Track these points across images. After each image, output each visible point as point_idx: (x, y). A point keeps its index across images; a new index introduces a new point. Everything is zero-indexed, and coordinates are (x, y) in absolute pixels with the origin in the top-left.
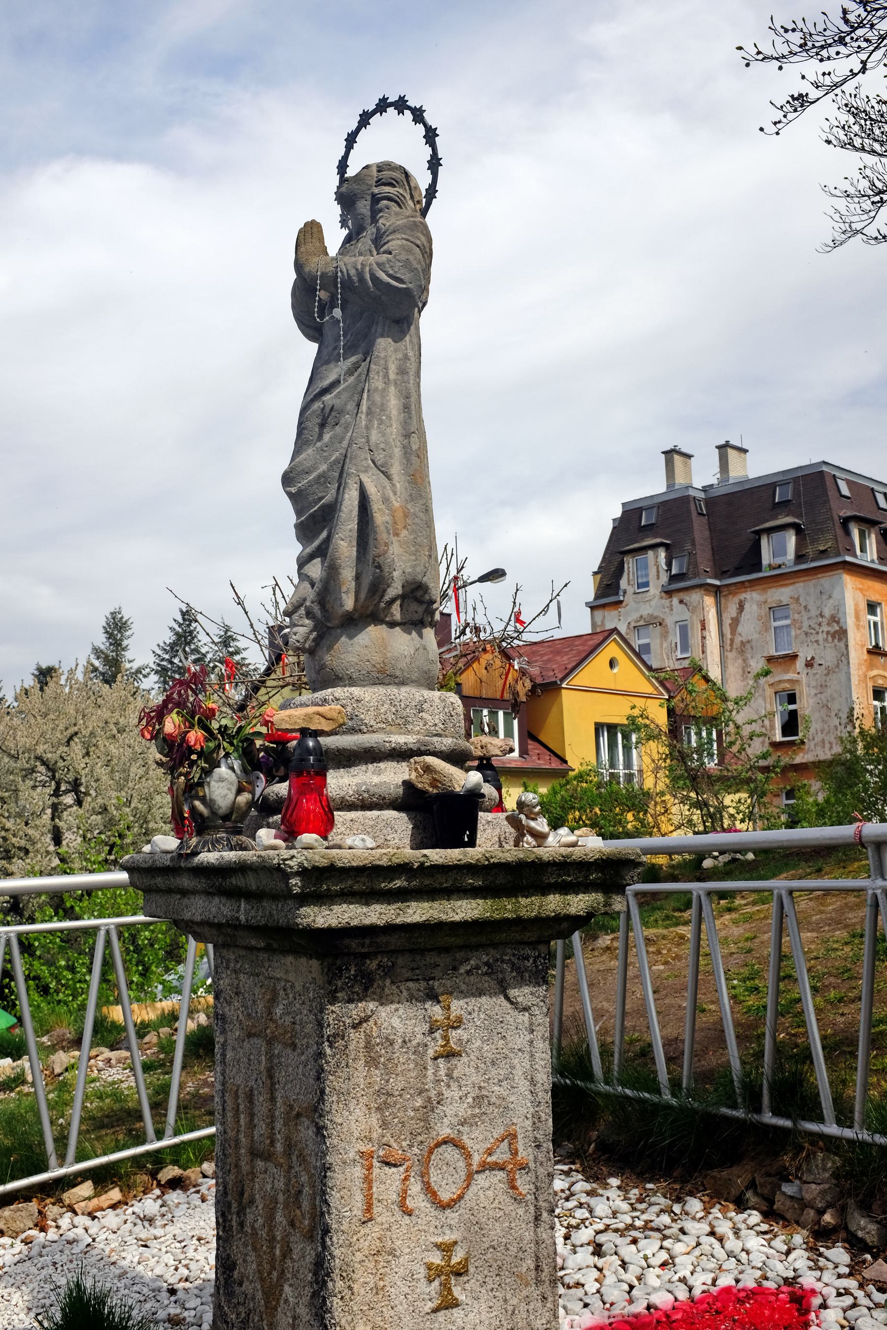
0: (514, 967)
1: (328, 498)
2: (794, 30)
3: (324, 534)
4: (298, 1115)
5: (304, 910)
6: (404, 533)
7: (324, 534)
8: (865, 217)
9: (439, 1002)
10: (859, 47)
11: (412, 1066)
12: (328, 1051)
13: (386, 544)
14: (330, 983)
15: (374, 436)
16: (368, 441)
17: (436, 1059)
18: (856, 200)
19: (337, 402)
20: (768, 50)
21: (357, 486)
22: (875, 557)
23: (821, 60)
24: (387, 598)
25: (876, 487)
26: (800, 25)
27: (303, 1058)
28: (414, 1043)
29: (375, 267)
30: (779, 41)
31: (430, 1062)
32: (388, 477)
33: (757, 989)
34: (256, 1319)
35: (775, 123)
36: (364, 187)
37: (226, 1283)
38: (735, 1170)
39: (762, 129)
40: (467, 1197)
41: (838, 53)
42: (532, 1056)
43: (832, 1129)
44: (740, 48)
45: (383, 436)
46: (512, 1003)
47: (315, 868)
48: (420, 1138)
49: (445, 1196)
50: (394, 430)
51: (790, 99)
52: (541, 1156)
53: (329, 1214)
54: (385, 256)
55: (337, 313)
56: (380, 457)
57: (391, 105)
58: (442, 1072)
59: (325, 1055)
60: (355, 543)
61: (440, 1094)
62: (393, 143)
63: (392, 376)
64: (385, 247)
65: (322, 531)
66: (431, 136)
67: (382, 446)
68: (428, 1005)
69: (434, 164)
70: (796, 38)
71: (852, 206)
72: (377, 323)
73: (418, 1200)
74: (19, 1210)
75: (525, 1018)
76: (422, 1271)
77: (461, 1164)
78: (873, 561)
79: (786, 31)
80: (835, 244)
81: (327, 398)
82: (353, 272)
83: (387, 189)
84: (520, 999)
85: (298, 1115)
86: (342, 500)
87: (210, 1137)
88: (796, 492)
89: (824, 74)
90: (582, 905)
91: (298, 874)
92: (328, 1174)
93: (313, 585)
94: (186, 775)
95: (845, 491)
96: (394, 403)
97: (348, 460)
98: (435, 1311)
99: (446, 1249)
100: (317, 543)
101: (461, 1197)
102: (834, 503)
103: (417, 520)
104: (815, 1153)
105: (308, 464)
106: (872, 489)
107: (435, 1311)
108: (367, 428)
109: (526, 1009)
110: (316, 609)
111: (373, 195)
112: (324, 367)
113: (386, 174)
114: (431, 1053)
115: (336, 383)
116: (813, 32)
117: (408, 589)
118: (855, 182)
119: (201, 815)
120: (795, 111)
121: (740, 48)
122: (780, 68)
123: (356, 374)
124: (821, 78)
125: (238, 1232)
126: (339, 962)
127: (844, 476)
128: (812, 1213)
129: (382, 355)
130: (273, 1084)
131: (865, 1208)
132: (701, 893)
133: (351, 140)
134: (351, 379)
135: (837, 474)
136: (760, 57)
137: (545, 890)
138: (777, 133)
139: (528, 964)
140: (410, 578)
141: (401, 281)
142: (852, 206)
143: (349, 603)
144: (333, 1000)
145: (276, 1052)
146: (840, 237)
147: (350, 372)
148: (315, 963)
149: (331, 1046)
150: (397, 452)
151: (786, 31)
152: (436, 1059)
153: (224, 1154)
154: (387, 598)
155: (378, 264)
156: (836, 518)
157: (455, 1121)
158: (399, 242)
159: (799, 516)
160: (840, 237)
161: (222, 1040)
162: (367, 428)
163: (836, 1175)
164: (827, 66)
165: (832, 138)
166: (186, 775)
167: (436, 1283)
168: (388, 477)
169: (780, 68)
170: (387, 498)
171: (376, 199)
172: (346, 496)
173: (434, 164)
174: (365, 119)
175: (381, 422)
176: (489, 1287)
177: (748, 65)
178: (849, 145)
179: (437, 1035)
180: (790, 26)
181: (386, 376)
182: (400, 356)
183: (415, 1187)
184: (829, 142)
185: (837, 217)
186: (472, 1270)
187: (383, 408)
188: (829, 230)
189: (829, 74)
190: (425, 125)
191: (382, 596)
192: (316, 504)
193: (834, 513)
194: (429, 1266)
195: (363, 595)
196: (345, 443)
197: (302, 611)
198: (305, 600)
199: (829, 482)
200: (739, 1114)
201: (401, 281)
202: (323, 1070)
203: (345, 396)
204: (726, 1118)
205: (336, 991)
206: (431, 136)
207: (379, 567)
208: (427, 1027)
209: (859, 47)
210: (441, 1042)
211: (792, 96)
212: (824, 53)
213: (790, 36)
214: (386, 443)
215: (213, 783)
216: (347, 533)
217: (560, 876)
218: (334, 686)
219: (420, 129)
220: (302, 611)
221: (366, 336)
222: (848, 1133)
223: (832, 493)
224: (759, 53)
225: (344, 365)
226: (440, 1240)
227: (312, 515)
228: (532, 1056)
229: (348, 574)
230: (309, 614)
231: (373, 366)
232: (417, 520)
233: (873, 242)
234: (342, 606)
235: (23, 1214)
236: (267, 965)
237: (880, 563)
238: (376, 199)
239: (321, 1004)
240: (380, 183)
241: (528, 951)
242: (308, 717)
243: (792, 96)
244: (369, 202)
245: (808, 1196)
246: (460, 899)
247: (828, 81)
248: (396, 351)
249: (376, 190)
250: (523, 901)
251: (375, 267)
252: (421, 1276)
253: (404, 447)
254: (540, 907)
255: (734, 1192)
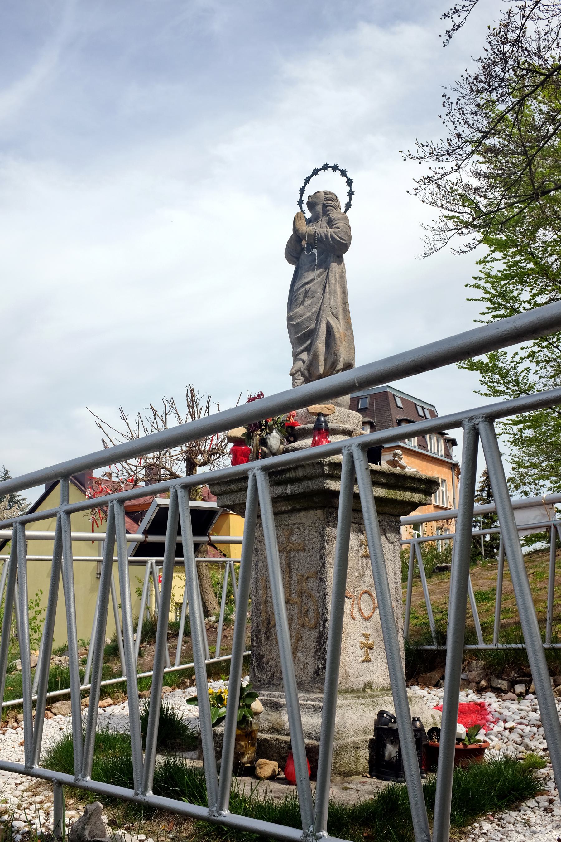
0: (389, 525)
1: (312, 326)
2: (427, 146)
3: (309, 342)
4: (308, 578)
5: (327, 481)
6: (344, 343)
7: (309, 342)
8: (442, 242)
9: (363, 534)
10: (456, 157)
11: (354, 559)
12: (327, 546)
13: (339, 346)
14: (327, 518)
15: (332, 302)
16: (330, 304)
17: (362, 557)
18: (437, 233)
19: (313, 288)
20: (415, 155)
21: (325, 322)
22: (416, 444)
23: (439, 161)
24: (337, 369)
25: (418, 403)
26: (430, 144)
27: (310, 554)
28: (355, 549)
29: (333, 233)
30: (420, 150)
31: (360, 558)
32: (338, 319)
33: (417, 617)
34: (278, 675)
35: (415, 189)
36: (319, 200)
37: (258, 664)
38: (434, 673)
39: (408, 192)
40: (373, 617)
41: (447, 159)
42: (395, 563)
43: (482, 646)
44: (401, 152)
45: (336, 302)
46: (388, 539)
47: (335, 463)
48: (357, 589)
49: (366, 615)
50: (339, 300)
51: (422, 178)
52: (399, 605)
53: (327, 613)
54: (337, 230)
55: (315, 251)
56: (335, 311)
57: (330, 167)
58: (364, 563)
59: (325, 548)
60: (324, 345)
61: (364, 572)
62: (331, 183)
63: (337, 279)
64: (336, 226)
65: (308, 340)
66: (349, 182)
67: (335, 306)
68: (359, 534)
69: (351, 194)
70: (428, 150)
71: (435, 236)
72: (330, 257)
73: (357, 615)
74: (63, 704)
75: (392, 547)
76: (358, 645)
77: (371, 603)
78: (414, 447)
79: (423, 146)
80: (426, 255)
81: (308, 286)
82: (323, 235)
83: (330, 202)
84: (391, 538)
85: (308, 578)
86: (320, 327)
87: (150, 677)
88: (371, 403)
89: (439, 168)
90: (417, 498)
91: (328, 465)
92: (327, 597)
93: (304, 362)
94: (260, 435)
95: (400, 404)
96: (339, 290)
97: (321, 311)
98: (363, 662)
99: (366, 636)
100: (305, 346)
101: (371, 616)
102: (393, 411)
103: (349, 338)
104: (472, 662)
105: (301, 313)
106: (415, 404)
107: (363, 662)
108: (329, 299)
109: (392, 543)
110: (306, 373)
111: (324, 204)
112: (306, 273)
113: (329, 196)
114: (360, 555)
115: (313, 280)
116: (436, 148)
117: (345, 366)
118: (438, 223)
119: (265, 452)
120: (425, 184)
121: (401, 152)
122: (420, 163)
123: (321, 277)
124: (438, 170)
125: (265, 641)
126: (330, 510)
127: (399, 395)
128: (474, 684)
129: (334, 270)
130: (290, 570)
131: (499, 677)
132: (415, 543)
133: (308, 180)
134: (319, 279)
135: (396, 394)
136: (411, 157)
137: (405, 489)
138: (416, 195)
139: (393, 524)
140: (346, 361)
141: (344, 240)
142: (435, 236)
143: (321, 370)
144: (328, 526)
145: (292, 556)
146: (429, 252)
147: (319, 276)
148: (319, 512)
149: (327, 544)
150: (341, 310)
151: (423, 146)
152: (362, 557)
153: (257, 609)
154: (337, 369)
155: (334, 232)
156: (394, 420)
157: (368, 584)
158: (342, 224)
159: (373, 417)
160: (429, 252)
161: (256, 559)
162: (329, 299)
163: (483, 668)
164: (441, 164)
165: (425, 199)
166: (260, 435)
167: (363, 650)
168: (338, 319)
169: (420, 163)
170: (339, 328)
171: (325, 206)
172: (321, 326)
173: (351, 194)
174: (316, 172)
175: (335, 297)
176: (381, 656)
177: (405, 160)
178: (434, 203)
179: (363, 547)
180: (425, 144)
181: (335, 278)
182: (340, 271)
183: (356, 609)
184: (423, 201)
185: (427, 241)
186: (375, 648)
187: (335, 291)
188: (422, 248)
189: (442, 168)
190: (347, 177)
191: (335, 368)
192: (305, 329)
193: (393, 416)
194: (361, 643)
195: (328, 367)
196: (319, 305)
197: (299, 373)
198: (300, 369)
199: (390, 398)
200: (434, 647)
201: (344, 240)
202: (324, 554)
203: (316, 286)
204: (426, 650)
205: (329, 522)
206: (349, 182)
207: (336, 355)
208: (359, 543)
209: (456, 157)
210: (364, 551)
211: (424, 177)
212: (441, 159)
213: (425, 148)
214: (337, 305)
215: (271, 439)
216: (322, 341)
217: (411, 484)
218: (314, 404)
219: (345, 179)
220: (299, 373)
221: (325, 262)
222: (492, 646)
223: (392, 405)
224: (410, 155)
225: (317, 272)
226: (364, 633)
227: (304, 334)
228: (395, 563)
229: (322, 358)
230: (303, 374)
231: (330, 274)
232: (349, 338)
233: (456, 253)
234: (318, 371)
235: (66, 706)
236: (288, 519)
237: (419, 448)
238: (325, 206)
239: (323, 527)
240: (326, 199)
241: (393, 519)
242: (322, 409)
243: (424, 177)
244: (321, 207)
245: (471, 677)
246: (377, 487)
247: (441, 171)
248: (338, 269)
249: (325, 202)
250: (398, 493)
251: (333, 233)
252: (358, 646)
253: (343, 308)
254: (404, 496)
255: (434, 682)
